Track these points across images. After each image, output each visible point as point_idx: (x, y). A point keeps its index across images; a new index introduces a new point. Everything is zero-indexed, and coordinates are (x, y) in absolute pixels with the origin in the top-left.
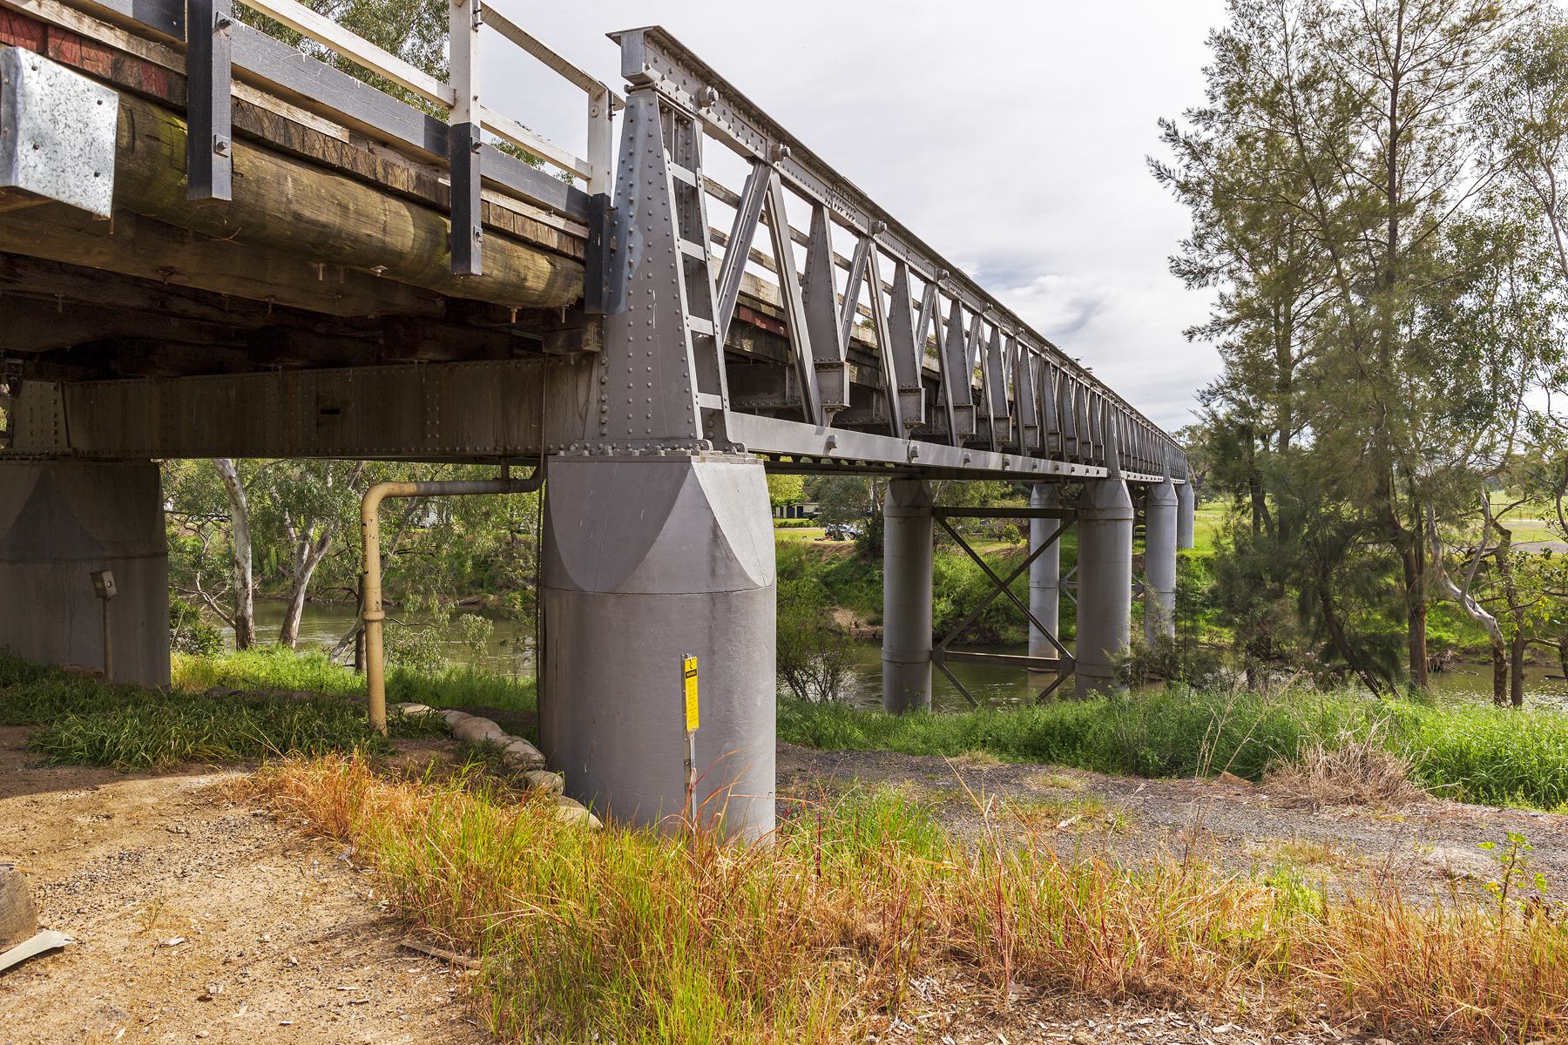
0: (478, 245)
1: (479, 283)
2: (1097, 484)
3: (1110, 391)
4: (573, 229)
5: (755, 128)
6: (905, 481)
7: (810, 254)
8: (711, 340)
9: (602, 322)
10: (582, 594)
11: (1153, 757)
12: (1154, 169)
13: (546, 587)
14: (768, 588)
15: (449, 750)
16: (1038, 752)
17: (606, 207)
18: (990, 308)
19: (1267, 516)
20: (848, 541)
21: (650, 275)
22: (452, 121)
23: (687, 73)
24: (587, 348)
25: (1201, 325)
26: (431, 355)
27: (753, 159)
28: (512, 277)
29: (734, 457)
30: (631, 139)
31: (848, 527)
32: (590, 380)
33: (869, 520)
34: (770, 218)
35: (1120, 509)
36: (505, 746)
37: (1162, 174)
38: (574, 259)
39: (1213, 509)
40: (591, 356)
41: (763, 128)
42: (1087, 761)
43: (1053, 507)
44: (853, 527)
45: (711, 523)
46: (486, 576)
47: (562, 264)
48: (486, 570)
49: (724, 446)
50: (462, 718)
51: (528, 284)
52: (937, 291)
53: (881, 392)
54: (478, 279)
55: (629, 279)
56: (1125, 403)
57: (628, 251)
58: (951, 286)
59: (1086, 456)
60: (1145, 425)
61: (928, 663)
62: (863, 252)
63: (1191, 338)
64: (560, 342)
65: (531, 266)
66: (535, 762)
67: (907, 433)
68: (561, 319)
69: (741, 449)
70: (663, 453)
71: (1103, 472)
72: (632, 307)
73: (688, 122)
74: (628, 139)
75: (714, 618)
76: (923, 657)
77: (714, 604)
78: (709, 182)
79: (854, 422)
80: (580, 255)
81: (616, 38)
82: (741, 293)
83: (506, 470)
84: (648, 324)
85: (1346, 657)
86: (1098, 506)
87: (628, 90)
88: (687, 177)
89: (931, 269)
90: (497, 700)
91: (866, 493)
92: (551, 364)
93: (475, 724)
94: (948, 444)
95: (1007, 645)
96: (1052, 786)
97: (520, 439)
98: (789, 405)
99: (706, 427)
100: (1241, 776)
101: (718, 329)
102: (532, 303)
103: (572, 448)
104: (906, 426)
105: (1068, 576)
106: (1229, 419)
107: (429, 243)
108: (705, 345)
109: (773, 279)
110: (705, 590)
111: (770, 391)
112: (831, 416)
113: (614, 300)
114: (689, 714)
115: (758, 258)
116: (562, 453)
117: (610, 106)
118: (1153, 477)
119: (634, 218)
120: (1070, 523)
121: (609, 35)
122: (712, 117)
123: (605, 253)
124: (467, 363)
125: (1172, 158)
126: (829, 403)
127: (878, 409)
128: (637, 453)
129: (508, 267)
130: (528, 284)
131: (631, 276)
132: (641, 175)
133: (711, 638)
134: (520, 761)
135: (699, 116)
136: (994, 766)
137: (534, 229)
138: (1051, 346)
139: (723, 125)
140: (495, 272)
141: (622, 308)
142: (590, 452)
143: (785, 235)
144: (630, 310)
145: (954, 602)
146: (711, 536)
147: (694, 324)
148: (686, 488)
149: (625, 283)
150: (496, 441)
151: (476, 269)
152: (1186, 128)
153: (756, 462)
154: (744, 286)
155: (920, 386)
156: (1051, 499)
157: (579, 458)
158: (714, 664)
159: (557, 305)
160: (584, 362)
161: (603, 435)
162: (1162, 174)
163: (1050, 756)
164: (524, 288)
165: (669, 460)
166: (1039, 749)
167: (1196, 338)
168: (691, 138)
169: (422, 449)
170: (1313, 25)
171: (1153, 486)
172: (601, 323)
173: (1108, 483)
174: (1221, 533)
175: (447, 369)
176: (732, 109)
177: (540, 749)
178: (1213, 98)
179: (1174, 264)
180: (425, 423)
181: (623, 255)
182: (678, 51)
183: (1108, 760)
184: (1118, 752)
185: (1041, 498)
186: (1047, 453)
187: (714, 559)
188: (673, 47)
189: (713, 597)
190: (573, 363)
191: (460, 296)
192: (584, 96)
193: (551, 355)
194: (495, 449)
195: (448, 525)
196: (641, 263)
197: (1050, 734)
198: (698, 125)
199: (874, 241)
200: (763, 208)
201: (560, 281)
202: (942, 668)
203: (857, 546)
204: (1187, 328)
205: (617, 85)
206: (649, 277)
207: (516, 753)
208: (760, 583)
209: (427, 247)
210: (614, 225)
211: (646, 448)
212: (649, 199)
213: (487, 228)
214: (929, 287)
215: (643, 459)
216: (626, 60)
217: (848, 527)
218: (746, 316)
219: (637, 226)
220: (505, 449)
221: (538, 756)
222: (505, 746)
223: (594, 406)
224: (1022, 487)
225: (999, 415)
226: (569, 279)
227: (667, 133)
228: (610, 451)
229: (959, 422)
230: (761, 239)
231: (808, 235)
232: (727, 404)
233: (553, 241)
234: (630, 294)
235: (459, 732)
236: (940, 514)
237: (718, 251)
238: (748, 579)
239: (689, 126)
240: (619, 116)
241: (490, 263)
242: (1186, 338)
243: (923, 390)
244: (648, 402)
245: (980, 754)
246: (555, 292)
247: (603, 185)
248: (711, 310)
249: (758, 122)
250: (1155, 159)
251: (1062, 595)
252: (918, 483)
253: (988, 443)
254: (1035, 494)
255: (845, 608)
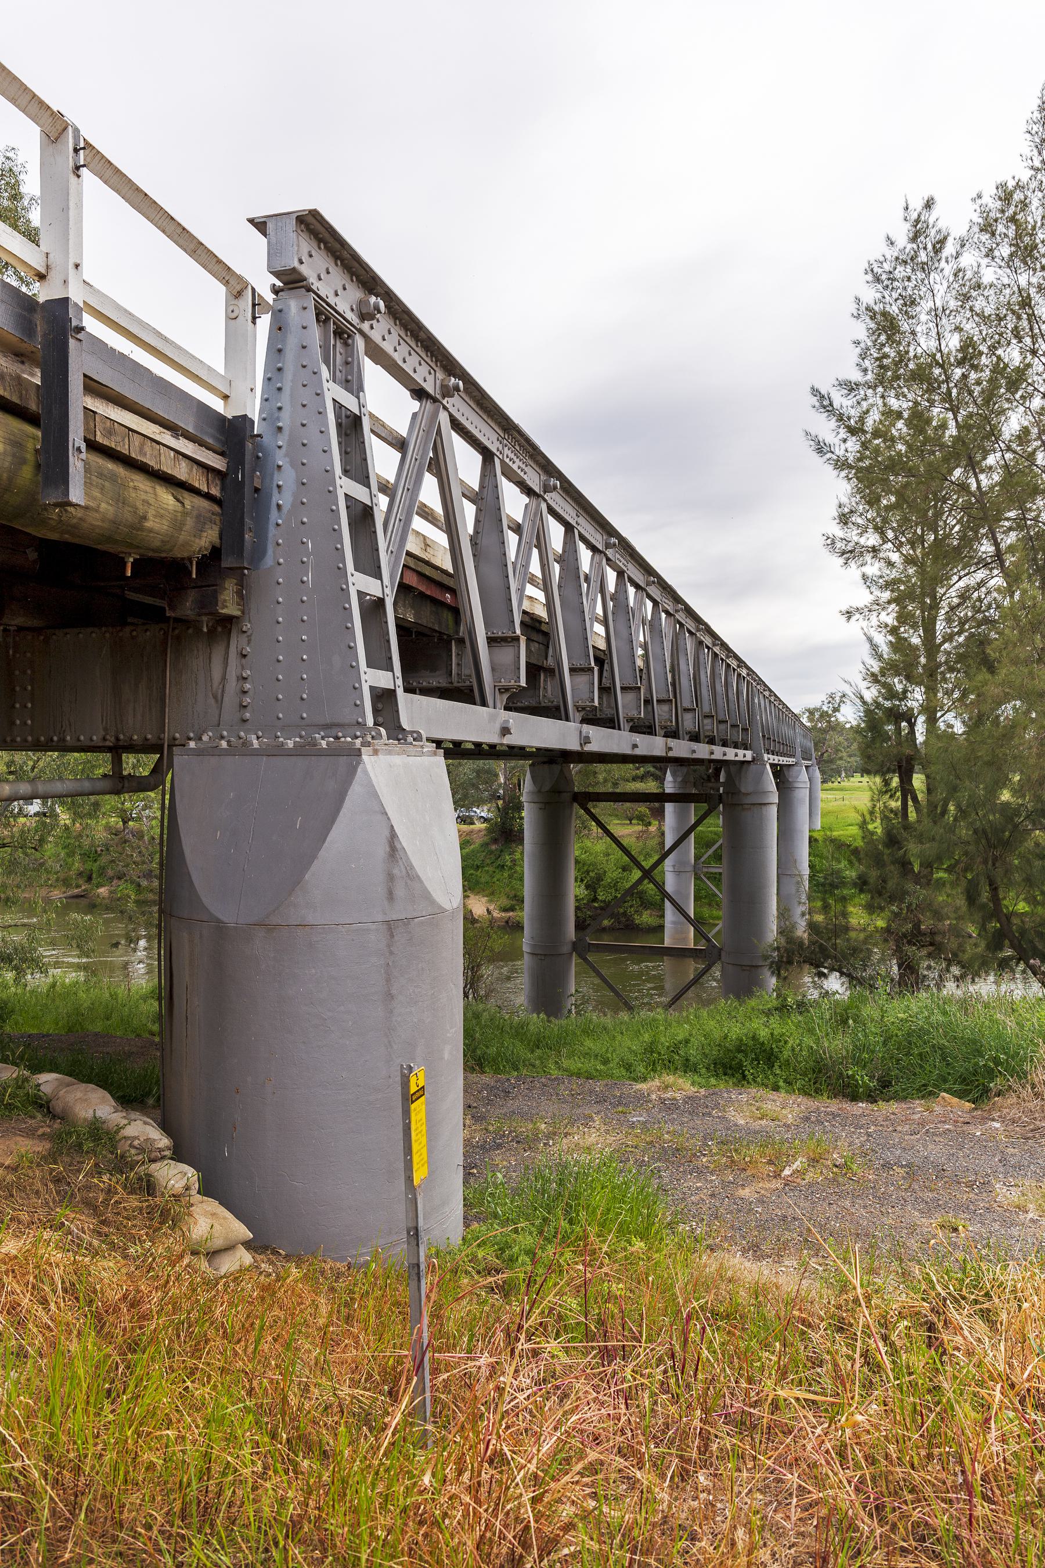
0: (80, 465)
1: (80, 519)
2: (741, 768)
3: (754, 672)
4: (209, 459)
5: (423, 355)
6: (546, 766)
7: (479, 511)
8: (380, 602)
9: (242, 580)
10: (220, 928)
11: (863, 1078)
12: (812, 443)
13: (171, 916)
14: (454, 911)
15: (43, 1134)
16: (729, 1072)
17: (248, 434)
18: (654, 582)
19: (915, 799)
20: (479, 826)
21: (305, 520)
22: (42, 293)
23: (347, 277)
24: (224, 611)
25: (861, 605)
26: (19, 621)
27: (419, 393)
28: (127, 515)
29: (411, 748)
30: (280, 351)
31: (478, 811)
32: (227, 653)
33: (500, 802)
34: (439, 466)
35: (766, 793)
36: (119, 1128)
37: (821, 448)
38: (208, 496)
39: (831, 789)
40: (228, 624)
41: (432, 356)
42: (788, 1082)
43: (687, 791)
44: (483, 812)
45: (386, 833)
46: (95, 867)
47: (191, 501)
48: (95, 861)
49: (397, 732)
50: (61, 1084)
51: (148, 524)
52: (604, 561)
53: (550, 672)
54: (79, 513)
55: (278, 525)
56: (765, 685)
57: (275, 491)
58: (618, 556)
59: (735, 739)
60: (780, 707)
61: (571, 954)
62: (535, 518)
63: (849, 618)
64: (188, 607)
65: (152, 501)
66: (160, 1150)
67: (579, 716)
68: (191, 573)
69: (418, 738)
70: (324, 744)
71: (749, 755)
72: (281, 560)
73: (349, 336)
74: (276, 351)
75: (391, 953)
76: (566, 949)
77: (392, 936)
78: (371, 415)
79: (519, 704)
80: (215, 491)
81: (260, 225)
82: (408, 554)
83: (117, 763)
84: (303, 582)
85: (1012, 946)
86: (743, 790)
87: (276, 291)
88: (350, 402)
89: (599, 536)
90: (108, 1018)
91: (497, 775)
92: (177, 632)
93: (79, 1095)
94: (614, 728)
95: (642, 929)
96: (761, 1119)
97: (136, 728)
98: (456, 684)
99: (376, 711)
100: (960, 1098)
101: (387, 591)
102: (153, 550)
103: (205, 738)
104: (578, 708)
105: (703, 859)
106: (875, 702)
107: (9, 459)
108: (373, 608)
109: (441, 538)
110: (380, 918)
111: (433, 669)
112: (505, 696)
113: (259, 551)
114: (416, 1159)
115: (426, 514)
116: (192, 744)
117: (254, 305)
118: (781, 758)
119: (284, 449)
120: (715, 808)
121: (251, 221)
122: (376, 336)
123: (248, 491)
124: (68, 630)
125: (827, 429)
126: (503, 683)
127: (547, 689)
128: (290, 744)
129: (121, 500)
130: (148, 524)
131: (280, 521)
132: (291, 395)
133: (388, 980)
134: (141, 1150)
135: (361, 332)
136: (690, 1093)
137: (156, 453)
138: (706, 624)
139: (388, 347)
140: (103, 505)
141: (269, 561)
142: (229, 742)
143: (456, 491)
144: (279, 564)
145: (587, 887)
146: (388, 849)
147: (360, 583)
148: (356, 789)
149: (272, 531)
150: (105, 729)
151: (76, 494)
152: (841, 400)
153: (435, 754)
154: (412, 545)
155: (593, 664)
156: (685, 782)
157: (214, 751)
158: (391, 1012)
159: (186, 555)
160: (219, 629)
161: (245, 721)
162: (821, 448)
163: (744, 1077)
164: (141, 529)
165: (332, 752)
166: (731, 1068)
167: (854, 618)
168: (352, 356)
169: (8, 739)
170: (966, 298)
171: (784, 768)
172: (241, 583)
173: (753, 767)
174: (868, 817)
175: (42, 638)
176: (398, 328)
177: (165, 1127)
178: (865, 371)
179: (829, 541)
180: (13, 707)
181: (270, 496)
182: (338, 246)
183: (810, 1080)
184: (820, 1071)
185: (675, 781)
186: (702, 737)
187: (391, 878)
188: (331, 240)
189: (390, 927)
190: (205, 630)
191: (54, 536)
192: (220, 291)
193: (177, 620)
194: (104, 739)
195: (54, 816)
196: (292, 506)
197: (742, 1051)
198: (360, 343)
199: (545, 500)
200: (431, 455)
201: (190, 522)
202: (585, 959)
203: (489, 831)
204: (844, 609)
205: (264, 283)
206: (303, 523)
207: (137, 1138)
208: (447, 906)
209: (7, 464)
210: (258, 457)
211: (301, 737)
212: (303, 425)
213: (93, 446)
214: (597, 557)
215: (299, 751)
216: (272, 253)
217: (478, 811)
218: (412, 580)
219: (287, 459)
220: (117, 739)
221: (163, 1141)
222: (119, 1128)
223: (232, 685)
224: (652, 769)
225: (661, 697)
226: (201, 522)
227: (325, 348)
228: (255, 742)
229: (625, 704)
230: (429, 492)
231: (477, 489)
232: (399, 682)
233: (182, 471)
234: (278, 544)
235: (58, 1106)
236: (585, 799)
237: (383, 501)
238: (432, 902)
239: (350, 341)
240: (265, 321)
241: (97, 494)
242: (844, 618)
243: (596, 669)
244: (302, 679)
245: (670, 1079)
246: (183, 537)
247: (245, 406)
248: (379, 567)
249: (426, 349)
250: (813, 434)
251: (697, 878)
252: (559, 767)
253: (650, 727)
254: (669, 777)
255: (478, 893)
